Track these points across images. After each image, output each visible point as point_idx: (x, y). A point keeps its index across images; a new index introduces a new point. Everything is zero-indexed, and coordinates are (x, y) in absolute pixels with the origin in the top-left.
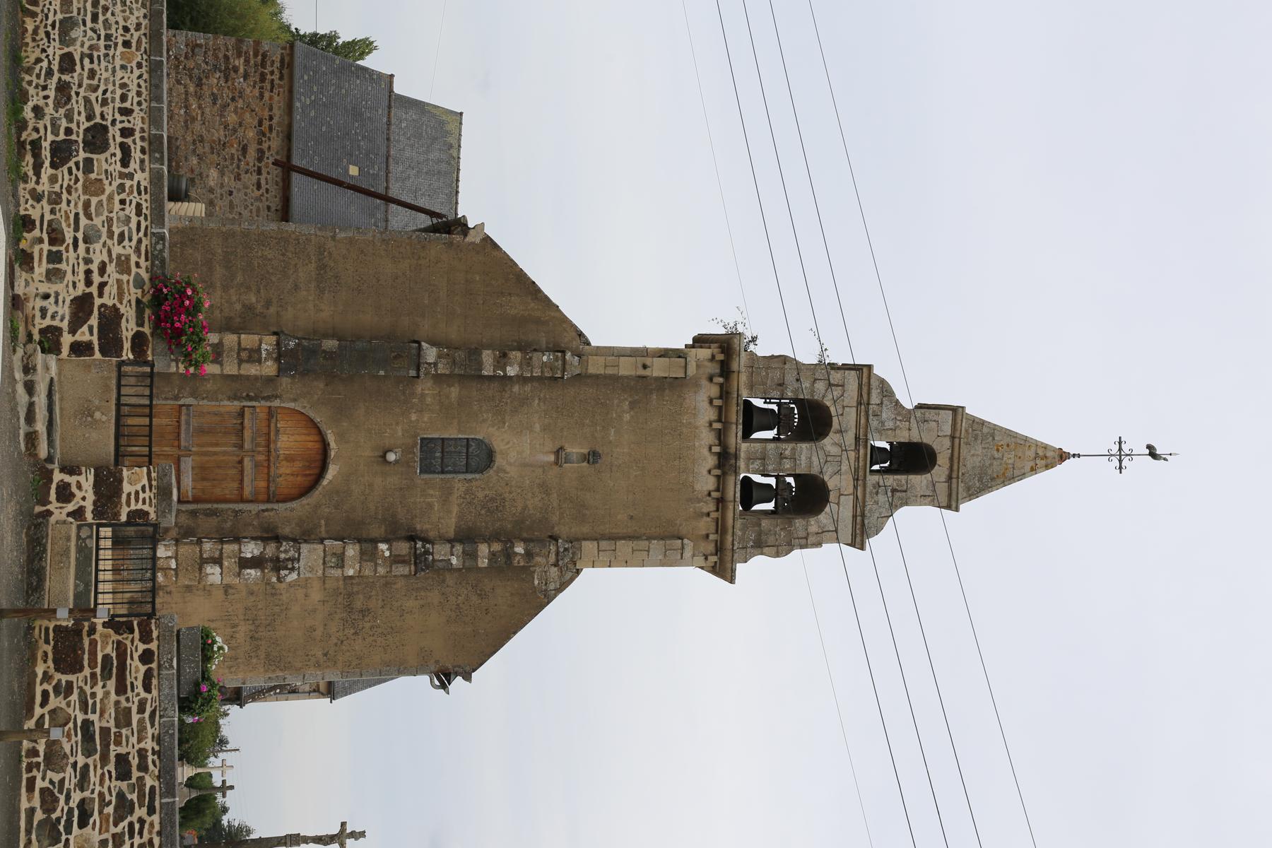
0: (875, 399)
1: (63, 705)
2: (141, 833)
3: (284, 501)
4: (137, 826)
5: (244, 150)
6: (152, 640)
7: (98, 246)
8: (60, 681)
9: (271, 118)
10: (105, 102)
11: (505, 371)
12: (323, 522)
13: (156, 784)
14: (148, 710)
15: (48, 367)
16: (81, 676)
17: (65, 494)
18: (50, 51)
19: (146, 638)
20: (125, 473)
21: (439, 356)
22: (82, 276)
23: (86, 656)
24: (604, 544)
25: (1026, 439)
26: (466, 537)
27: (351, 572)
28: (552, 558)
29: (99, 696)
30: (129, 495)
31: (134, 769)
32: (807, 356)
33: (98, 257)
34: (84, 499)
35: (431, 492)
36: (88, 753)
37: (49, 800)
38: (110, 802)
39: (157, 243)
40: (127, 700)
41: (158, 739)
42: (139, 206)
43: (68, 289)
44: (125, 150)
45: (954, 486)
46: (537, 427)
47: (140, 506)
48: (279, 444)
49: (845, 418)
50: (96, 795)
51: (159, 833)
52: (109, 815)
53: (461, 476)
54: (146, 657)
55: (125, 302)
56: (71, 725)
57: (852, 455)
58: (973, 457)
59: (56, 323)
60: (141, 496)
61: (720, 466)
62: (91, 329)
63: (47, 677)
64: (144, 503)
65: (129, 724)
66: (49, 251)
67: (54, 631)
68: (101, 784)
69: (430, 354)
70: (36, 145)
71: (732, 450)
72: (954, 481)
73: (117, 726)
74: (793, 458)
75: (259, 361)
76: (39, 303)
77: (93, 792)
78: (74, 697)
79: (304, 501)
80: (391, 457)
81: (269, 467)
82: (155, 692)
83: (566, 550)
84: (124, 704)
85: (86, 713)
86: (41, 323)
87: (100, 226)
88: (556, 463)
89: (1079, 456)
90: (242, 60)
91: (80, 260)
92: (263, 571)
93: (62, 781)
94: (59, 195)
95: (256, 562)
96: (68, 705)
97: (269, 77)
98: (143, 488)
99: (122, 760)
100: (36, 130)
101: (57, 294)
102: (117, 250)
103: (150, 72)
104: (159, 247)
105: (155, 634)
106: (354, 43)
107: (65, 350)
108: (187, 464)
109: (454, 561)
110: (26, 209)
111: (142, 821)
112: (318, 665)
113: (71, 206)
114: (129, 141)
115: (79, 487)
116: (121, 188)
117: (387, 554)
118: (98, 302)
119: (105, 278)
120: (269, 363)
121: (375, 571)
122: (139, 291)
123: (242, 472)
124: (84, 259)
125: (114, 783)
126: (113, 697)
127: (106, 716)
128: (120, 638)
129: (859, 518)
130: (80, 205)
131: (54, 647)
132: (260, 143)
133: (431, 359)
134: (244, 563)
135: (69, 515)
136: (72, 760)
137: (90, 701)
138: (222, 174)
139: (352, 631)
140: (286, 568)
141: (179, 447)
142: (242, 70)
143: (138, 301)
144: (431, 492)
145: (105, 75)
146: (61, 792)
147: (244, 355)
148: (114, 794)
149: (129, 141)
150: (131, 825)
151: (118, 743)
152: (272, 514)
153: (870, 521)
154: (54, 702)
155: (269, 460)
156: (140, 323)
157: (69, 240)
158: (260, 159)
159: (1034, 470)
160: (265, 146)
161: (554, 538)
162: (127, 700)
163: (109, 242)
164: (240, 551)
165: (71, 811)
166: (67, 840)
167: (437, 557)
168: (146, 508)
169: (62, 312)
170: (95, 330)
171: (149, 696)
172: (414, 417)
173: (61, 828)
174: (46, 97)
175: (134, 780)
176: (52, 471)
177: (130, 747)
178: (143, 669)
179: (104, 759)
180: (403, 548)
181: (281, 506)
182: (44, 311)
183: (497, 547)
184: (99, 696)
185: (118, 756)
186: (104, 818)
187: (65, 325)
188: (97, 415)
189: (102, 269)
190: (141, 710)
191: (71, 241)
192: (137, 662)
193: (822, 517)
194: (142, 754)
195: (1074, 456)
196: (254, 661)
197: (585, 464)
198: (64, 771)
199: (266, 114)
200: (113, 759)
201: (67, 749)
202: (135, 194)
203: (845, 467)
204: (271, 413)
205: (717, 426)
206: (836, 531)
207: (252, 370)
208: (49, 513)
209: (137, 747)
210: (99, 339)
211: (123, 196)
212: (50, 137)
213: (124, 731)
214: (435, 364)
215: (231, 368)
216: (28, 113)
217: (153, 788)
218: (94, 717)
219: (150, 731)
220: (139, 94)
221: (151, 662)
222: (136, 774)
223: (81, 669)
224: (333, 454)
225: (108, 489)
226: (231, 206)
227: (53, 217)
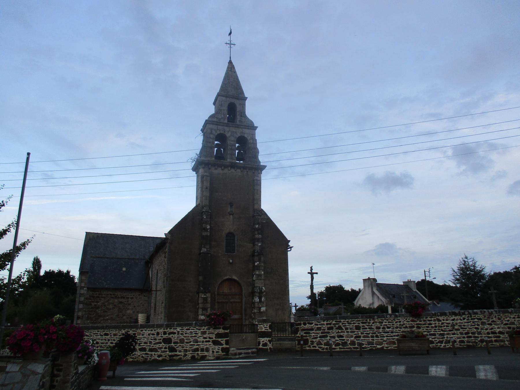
0: (215, 120)
5: (121, 303)
7: (199, 339)
9: (111, 294)
10: (155, 339)
15: (233, 350)
17: (265, 345)
18: (139, 354)
19: (300, 324)
20: (260, 330)
21: (204, 247)
22: (207, 343)
25: (226, 74)
26: (253, 241)
28: (259, 217)
33: (201, 339)
36: (327, 336)
37: (337, 345)
41: (324, 321)
42: (187, 329)
43: (210, 345)
44: (170, 334)
63: (310, 347)
69: (204, 250)
70: (170, 356)
76: (215, 353)
78: (314, 340)
86: (221, 352)
88: (233, 215)
94: (184, 350)
99: (329, 329)
100: (166, 356)
102: (200, 335)
103: (144, 328)
106: (34, 264)
107: (228, 346)
109: (260, 244)
111: (343, 324)
113: (188, 347)
114: (168, 333)
115: (263, 341)
116: (182, 334)
118: (214, 339)
126: (314, 331)
132: (118, 298)
133: (206, 250)
134: (260, 301)
138: (128, 309)
145: (146, 340)
149: (168, 333)
151: (325, 330)
154: (315, 345)
156: (220, 328)
157: (197, 347)
158: (124, 298)
160: (120, 296)
161: (254, 216)
174: (155, 354)
177: (325, 327)
178: (307, 325)
179: (328, 333)
180: (256, 258)
181: (244, 292)
183: (256, 232)
185: (328, 330)
186: (342, 332)
190: (317, 325)
194: (327, 324)
199: (109, 296)
203: (235, 131)
204: (218, 294)
205: (223, 168)
207: (209, 299)
208: (270, 348)
212: (168, 353)
215: (209, 305)
216: (160, 359)
218: (319, 335)
220: (152, 330)
222: (332, 325)
223: (308, 339)
225: (264, 334)
226: (138, 306)
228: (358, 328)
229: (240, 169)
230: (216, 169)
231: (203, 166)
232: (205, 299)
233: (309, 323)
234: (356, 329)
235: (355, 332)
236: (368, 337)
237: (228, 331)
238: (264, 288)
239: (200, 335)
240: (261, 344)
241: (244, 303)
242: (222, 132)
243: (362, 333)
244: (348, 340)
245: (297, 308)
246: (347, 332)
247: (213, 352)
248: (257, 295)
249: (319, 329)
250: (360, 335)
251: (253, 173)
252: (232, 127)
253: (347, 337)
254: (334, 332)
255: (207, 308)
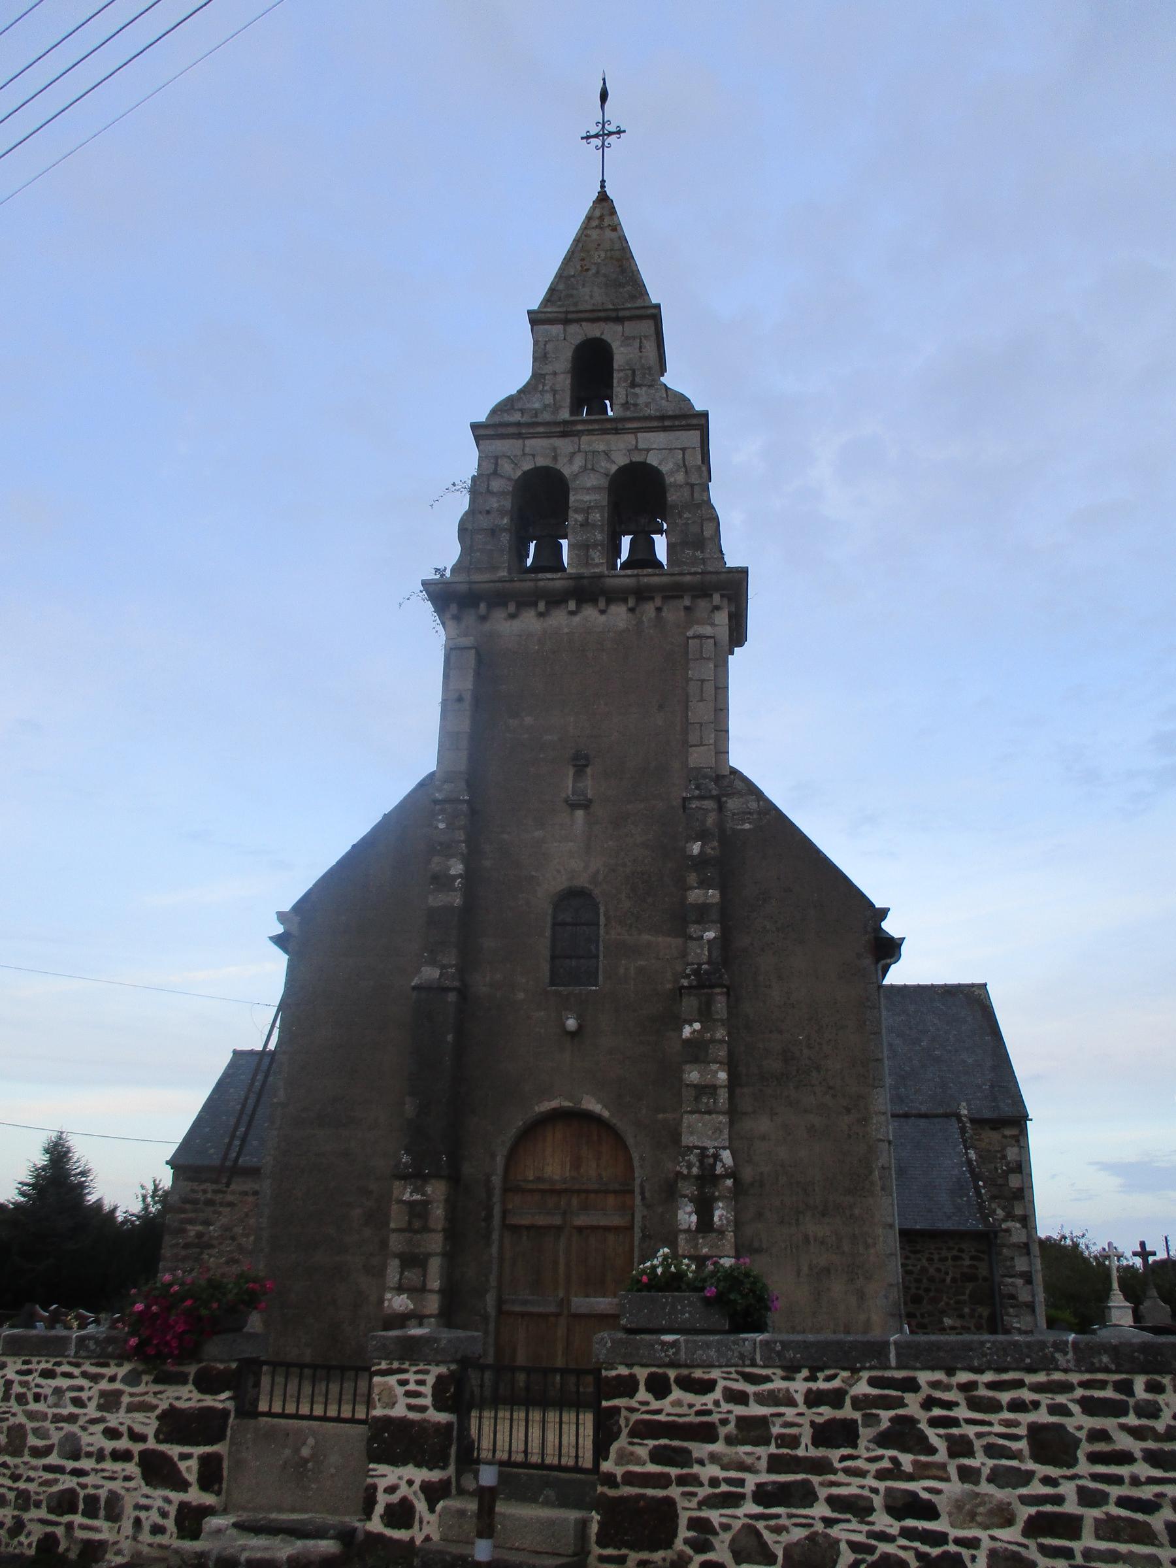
0: (516, 417)
1: (727, 1537)
2: (949, 1405)
3: (631, 1169)
4: (937, 1412)
6: (633, 1377)
7: (85, 1439)
8: (687, 1541)
11: (455, 877)
12: (660, 1116)
13: (865, 1375)
14: (741, 1386)
16: (681, 1503)
17: (401, 1514)
19: (628, 1387)
21: (433, 962)
22: (118, 1466)
23: (650, 1492)
24: (693, 738)
25: (577, 241)
26: (682, 919)
27: (723, 1076)
28: (709, 804)
29: (714, 1470)
30: (410, 1407)
31: (839, 1414)
32: (462, 503)
34: (410, 1483)
35: (622, 971)
36: (807, 1496)
38: (894, 1460)
39: (87, 1348)
40: (724, 1422)
41: (790, 1372)
45: (627, 313)
46: (538, 834)
47: (427, 1390)
48: (557, 1177)
49: (538, 452)
50: (881, 1486)
51: (950, 1372)
52: (915, 1463)
53: (602, 931)
54: (659, 1387)
55: (155, 1401)
56: (760, 1525)
57: (584, 439)
58: (592, 295)
59: (172, 1510)
60: (412, 1387)
61: (593, 600)
62: (184, 1457)
64: (421, 1383)
65: (763, 1421)
66: (84, 1514)
67: (604, 1546)
68: (862, 1474)
71: (571, 583)
72: (621, 314)
73: (767, 1443)
74: (587, 510)
75: (425, 1204)
76: (146, 1537)
77: (875, 1491)
78: (715, 1516)
79: (630, 1141)
80: (571, 1024)
81: (587, 1191)
82: (715, 1374)
83: (698, 787)
84: (731, 1428)
85: (742, 1497)
87: (62, 1434)
89: (603, 181)
90: (189, 1227)
91: (99, 1467)
92: (717, 1199)
93: (854, 1546)
95: (704, 1209)
96: (726, 1527)
97: (209, 1196)
98: (403, 1383)
99: (825, 1435)
101: (138, 1507)
102: (92, 1411)
104: (92, 1345)
105: (623, 1371)
108: (581, 1303)
109: (710, 935)
110: (30, 1545)
112: (864, 1120)
115: (391, 1490)
116: (21, 1399)
117: (697, 1026)
118: (151, 1444)
119: (123, 1429)
120: (429, 1189)
121: (722, 1041)
122: (145, 1378)
123: (594, 1228)
124: (99, 1461)
125: (862, 1451)
126: (718, 1447)
127: (749, 1460)
128: (625, 1431)
129: (667, 423)
130: (35, 1462)
131: (632, 1547)
134: (705, 1224)
135: (432, 1510)
136: (819, 1527)
137: (724, 1488)
139: (814, 1074)
140: (715, 1164)
141: (557, 1315)
142: (200, 1228)
143: (156, 1381)
144: (622, 971)
146: (871, 1550)
147: (417, 1224)
148: (880, 1452)
150: (934, 1422)
151: (794, 1442)
152: (647, 1187)
153: (670, 409)
155: (579, 1191)
156: (181, 1380)
159: (616, 227)
162: (724, 1422)
163: (81, 1422)
164: (688, 1231)
165: (907, 1533)
166: (958, 1541)
167: (705, 958)
168: (430, 1379)
169: (162, 1501)
170: (187, 1449)
171: (721, 1384)
172: (521, 996)
173: (935, 1552)
175: (857, 1415)
176: (369, 1534)
177: (800, 1419)
178: (677, 1393)
179: (821, 1467)
182: (157, 1530)
183: (692, 878)
184: (714, 1470)
185: (817, 1441)
187: (176, 1497)
188: (305, 1452)
189: (112, 1434)
190: (740, 1398)
191: (75, 1480)
192: (665, 1404)
193: (664, 469)
194: (814, 1399)
195: (603, 187)
196: (857, 1211)
197: (589, 770)
198: (838, 1541)
200: (820, 1452)
201: (798, 1534)
202: (29, 1378)
203: (601, 447)
206: (684, 450)
207: (438, 1212)
209: (802, 1408)
210: (198, 1444)
211: (30, 1397)
213: (776, 1430)
214: (443, 967)
215: (435, 1242)
217: (872, 1382)
219: (778, 1384)
221: (666, 1378)
222: (847, 1412)
223: (670, 1502)
224: (567, 1104)
227: (44, 1505)
228: (1051, 1445)
229: (625, 601)
230: (513, 616)
231: (454, 608)
232: (418, 1211)
233: (688, 1384)
234: (1037, 1458)
235: (1026, 1477)
236: (1145, 1535)
237: (221, 1400)
238: (726, 1155)
239: (92, 1411)
240: (379, 1509)
241: (638, 1235)
242: (541, 462)
243: (1088, 1498)
244: (973, 1543)
245: (1151, 1259)
246: (968, 1475)
247: (138, 1523)
248: (689, 1189)
249: (753, 1431)
250: (1071, 1507)
251: (687, 609)
252: (590, 432)
253: (966, 1512)
254: (862, 1471)
255: (428, 1255)
